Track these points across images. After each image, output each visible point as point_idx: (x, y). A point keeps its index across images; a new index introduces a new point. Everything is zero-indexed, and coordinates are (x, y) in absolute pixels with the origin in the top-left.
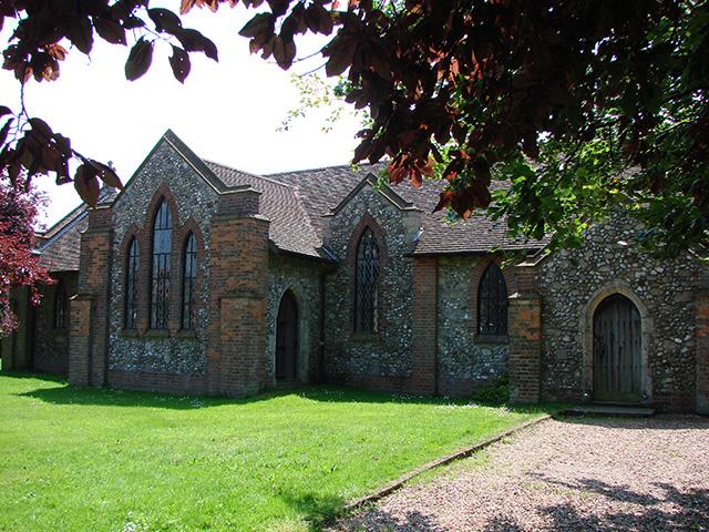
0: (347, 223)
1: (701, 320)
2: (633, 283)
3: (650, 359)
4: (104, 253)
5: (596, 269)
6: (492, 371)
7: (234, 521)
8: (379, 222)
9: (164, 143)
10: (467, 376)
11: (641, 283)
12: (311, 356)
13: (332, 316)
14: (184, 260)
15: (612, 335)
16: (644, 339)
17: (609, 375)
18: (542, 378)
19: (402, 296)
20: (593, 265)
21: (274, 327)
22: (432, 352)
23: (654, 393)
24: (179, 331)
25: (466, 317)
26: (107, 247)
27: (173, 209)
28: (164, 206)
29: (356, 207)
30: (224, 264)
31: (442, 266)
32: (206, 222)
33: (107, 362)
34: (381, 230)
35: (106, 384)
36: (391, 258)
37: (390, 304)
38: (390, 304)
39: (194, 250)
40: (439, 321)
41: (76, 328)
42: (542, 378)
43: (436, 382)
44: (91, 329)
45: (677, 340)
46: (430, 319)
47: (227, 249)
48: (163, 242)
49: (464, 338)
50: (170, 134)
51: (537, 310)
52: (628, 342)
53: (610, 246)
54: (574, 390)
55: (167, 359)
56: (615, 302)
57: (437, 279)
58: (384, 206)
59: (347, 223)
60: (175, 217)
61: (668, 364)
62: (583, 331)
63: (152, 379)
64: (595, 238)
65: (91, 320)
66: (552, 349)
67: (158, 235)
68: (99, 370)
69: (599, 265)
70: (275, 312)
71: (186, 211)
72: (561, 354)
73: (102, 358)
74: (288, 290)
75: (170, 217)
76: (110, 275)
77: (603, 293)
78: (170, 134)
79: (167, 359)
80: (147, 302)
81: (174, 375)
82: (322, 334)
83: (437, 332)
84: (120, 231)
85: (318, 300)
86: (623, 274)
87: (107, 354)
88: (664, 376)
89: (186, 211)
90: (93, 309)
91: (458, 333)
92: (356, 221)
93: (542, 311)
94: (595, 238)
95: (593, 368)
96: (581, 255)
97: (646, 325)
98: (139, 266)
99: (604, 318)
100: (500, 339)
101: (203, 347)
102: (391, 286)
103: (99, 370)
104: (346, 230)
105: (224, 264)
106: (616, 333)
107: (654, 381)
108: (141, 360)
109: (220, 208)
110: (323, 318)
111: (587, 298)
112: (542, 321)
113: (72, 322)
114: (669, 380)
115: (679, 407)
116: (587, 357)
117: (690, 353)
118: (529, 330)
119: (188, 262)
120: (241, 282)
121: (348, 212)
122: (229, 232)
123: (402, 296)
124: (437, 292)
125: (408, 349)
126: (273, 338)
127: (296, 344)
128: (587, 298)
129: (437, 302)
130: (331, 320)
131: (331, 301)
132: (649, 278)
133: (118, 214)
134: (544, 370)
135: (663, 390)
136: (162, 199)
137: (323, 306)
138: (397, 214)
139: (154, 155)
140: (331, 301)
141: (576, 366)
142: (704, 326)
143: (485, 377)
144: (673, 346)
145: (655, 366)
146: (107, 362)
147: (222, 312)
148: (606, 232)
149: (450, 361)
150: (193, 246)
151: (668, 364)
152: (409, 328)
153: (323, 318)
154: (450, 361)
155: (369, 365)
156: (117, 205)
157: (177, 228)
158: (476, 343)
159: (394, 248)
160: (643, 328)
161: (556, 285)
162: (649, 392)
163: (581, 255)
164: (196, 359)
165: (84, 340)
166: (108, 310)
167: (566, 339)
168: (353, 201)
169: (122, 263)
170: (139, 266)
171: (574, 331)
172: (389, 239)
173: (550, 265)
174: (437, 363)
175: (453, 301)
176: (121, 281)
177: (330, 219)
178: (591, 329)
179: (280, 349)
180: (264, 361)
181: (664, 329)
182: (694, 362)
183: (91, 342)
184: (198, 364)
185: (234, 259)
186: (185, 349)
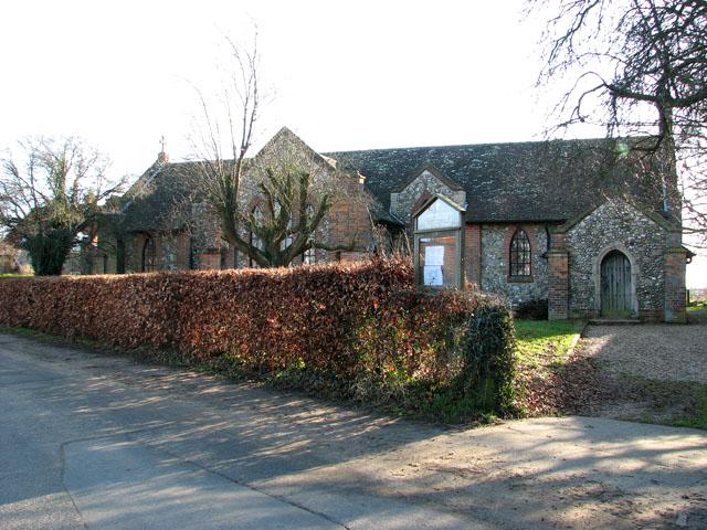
5: (603, 235)
11: (632, 244)
16: (633, 278)
18: (569, 302)
40: (482, 267)
42: (569, 302)
50: (285, 132)
61: (648, 293)
72: (581, 288)
77: (605, 250)
86: (622, 238)
92: (418, 196)
97: (635, 269)
141: (591, 294)
151: (648, 293)
160: (633, 271)
161: (579, 244)
173: (574, 231)
175: (492, 253)
181: (646, 271)
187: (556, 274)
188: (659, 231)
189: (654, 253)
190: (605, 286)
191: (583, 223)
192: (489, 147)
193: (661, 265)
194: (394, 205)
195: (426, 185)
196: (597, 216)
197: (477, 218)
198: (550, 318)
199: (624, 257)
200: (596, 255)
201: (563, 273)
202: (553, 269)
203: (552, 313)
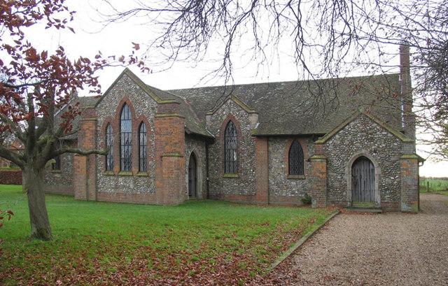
4: (92, 131)
7: (183, 282)
9: (125, 75)
11: (375, 152)
12: (203, 185)
13: (213, 165)
19: (249, 156)
22: (266, 183)
26: (94, 128)
27: (131, 107)
30: (163, 138)
32: (151, 117)
40: (269, 168)
46: (265, 167)
48: (127, 127)
49: (282, 176)
53: (360, 134)
55: (132, 186)
56: (361, 160)
60: (133, 114)
61: (388, 189)
68: (92, 191)
72: (337, 184)
74: (193, 152)
75: (130, 114)
77: (356, 154)
84: (101, 120)
86: (366, 147)
92: (224, 118)
97: (377, 171)
99: (357, 167)
100: (300, 177)
101: (152, 180)
106: (363, 175)
108: (116, 187)
109: (159, 111)
116: (349, 186)
126: (187, 176)
127: (196, 179)
134: (328, 190)
136: (125, 103)
137: (207, 159)
150: (144, 129)
151: (388, 189)
157: (134, 120)
160: (376, 172)
164: (149, 186)
167: (339, 177)
171: (343, 174)
173: (331, 142)
179: (190, 181)
181: (386, 173)
182: (400, 188)
186: (141, 181)
188: (396, 141)
189: (393, 159)
191: (337, 136)
192: (279, 84)
197: (264, 133)
201: (323, 173)
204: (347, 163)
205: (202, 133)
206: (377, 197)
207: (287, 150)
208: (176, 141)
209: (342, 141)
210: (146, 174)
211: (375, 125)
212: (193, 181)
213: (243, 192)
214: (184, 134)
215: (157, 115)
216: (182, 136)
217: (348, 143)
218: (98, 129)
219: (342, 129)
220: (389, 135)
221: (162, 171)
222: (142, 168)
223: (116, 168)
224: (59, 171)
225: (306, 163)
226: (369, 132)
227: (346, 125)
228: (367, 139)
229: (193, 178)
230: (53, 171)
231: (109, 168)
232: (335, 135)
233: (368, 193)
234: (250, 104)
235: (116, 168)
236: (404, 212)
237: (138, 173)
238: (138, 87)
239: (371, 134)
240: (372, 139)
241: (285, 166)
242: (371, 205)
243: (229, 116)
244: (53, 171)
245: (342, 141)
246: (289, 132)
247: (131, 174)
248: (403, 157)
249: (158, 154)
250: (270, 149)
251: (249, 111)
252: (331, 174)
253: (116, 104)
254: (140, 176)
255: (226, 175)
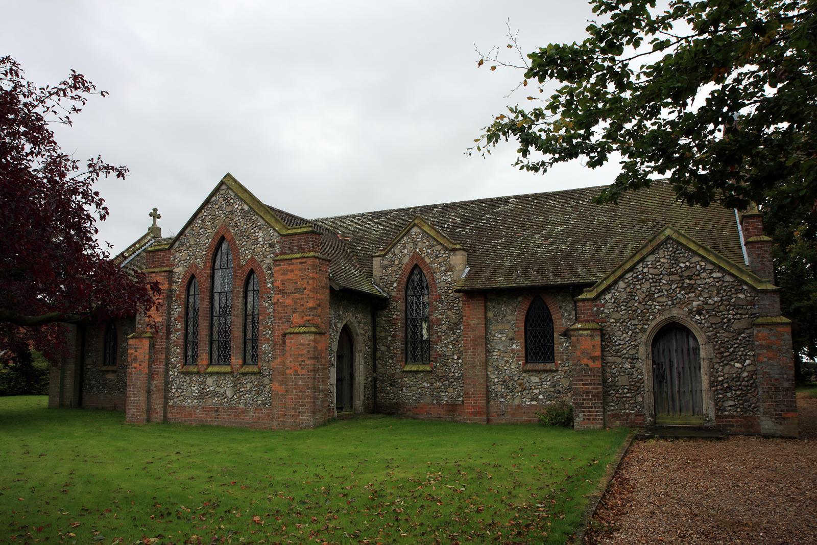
0: (397, 262)
1: (761, 345)
2: (690, 312)
3: (711, 384)
5: (653, 300)
6: (541, 397)
8: (428, 261)
9: (224, 187)
10: (517, 402)
11: (699, 312)
13: (383, 348)
14: (246, 297)
15: (671, 362)
16: (704, 365)
17: (670, 399)
18: (605, 403)
19: (451, 329)
20: (651, 296)
21: (334, 360)
23: (717, 416)
24: (241, 367)
25: (514, 347)
27: (233, 248)
28: (224, 246)
29: (404, 247)
30: (288, 300)
31: (430, 315)
32: (268, 261)
33: (166, 398)
34: (430, 269)
35: (165, 420)
36: (440, 295)
37: (440, 337)
38: (440, 337)
39: (255, 288)
40: (488, 352)
41: (134, 365)
42: (605, 403)
43: (488, 408)
44: (150, 366)
45: (737, 365)
46: (480, 351)
47: (290, 287)
48: (224, 281)
50: (228, 175)
51: (598, 339)
52: (687, 366)
53: (666, 278)
54: (637, 415)
55: (229, 393)
57: (486, 313)
58: (432, 246)
59: (397, 262)
60: (237, 257)
61: (729, 388)
62: (644, 358)
63: (214, 414)
64: (652, 271)
65: (150, 357)
66: (614, 376)
67: (218, 274)
68: (158, 406)
69: (656, 296)
70: (335, 347)
71: (247, 252)
72: (623, 380)
73: (161, 395)
76: (169, 313)
77: (655, 322)
78: (228, 175)
79: (229, 393)
80: (208, 338)
81: (237, 409)
82: (375, 366)
83: (487, 361)
84: (179, 270)
85: (370, 333)
86: (681, 303)
87: (166, 390)
88: (725, 399)
89: (247, 252)
90: (153, 346)
91: (507, 362)
92: (406, 260)
93: (602, 341)
94: (652, 271)
95: (654, 393)
96: (638, 287)
97: (705, 352)
98: (202, 305)
99: (662, 345)
100: (548, 366)
101: (266, 381)
102: (441, 320)
103: (158, 406)
104: (395, 268)
105: (288, 300)
107: (716, 404)
108: (202, 395)
109: (282, 247)
110: (375, 350)
111: (646, 327)
112: (603, 349)
113: (129, 359)
114: (731, 403)
115: (743, 429)
117: (750, 377)
118: (591, 358)
119: (250, 300)
120: (306, 318)
121: (397, 252)
122: (292, 270)
123: (451, 329)
124: (486, 324)
125: (459, 378)
126: (334, 370)
128: (646, 327)
129: (486, 334)
130: (383, 353)
131: (383, 334)
132: (706, 307)
133: (177, 254)
134: (606, 394)
135: (726, 413)
136: (223, 239)
137: (374, 339)
138: (445, 253)
139: (214, 198)
140: (383, 334)
141: (638, 391)
142: (765, 351)
143: (534, 403)
144: (733, 371)
145: (717, 390)
146: (166, 398)
147: (287, 348)
148: (662, 265)
149: (500, 388)
151: (729, 388)
152: (459, 358)
153: (375, 350)
154: (500, 388)
155: (421, 394)
156: (176, 246)
158: (525, 371)
159: (442, 284)
160: (703, 354)
161: (615, 316)
162: (712, 415)
163: (638, 287)
165: (143, 376)
166: (168, 347)
167: (627, 366)
168: (403, 242)
169: (183, 301)
170: (202, 305)
171: (635, 358)
172: (437, 275)
173: (608, 297)
174: (488, 391)
175: (501, 332)
176: (182, 318)
177: (380, 258)
178: (650, 356)
179: (339, 380)
180: (328, 394)
181: (723, 355)
182: (754, 386)
183: (150, 377)
184: (261, 399)
185: (298, 296)
186: (247, 384)
187: (584, 361)
188: (742, 291)
189: (736, 326)
190: (659, 377)
191: (621, 284)
192: (505, 200)
193: (749, 343)
194: (377, 272)
195: (415, 245)
196: (642, 273)
197: (479, 285)
198: (576, 426)
199: (687, 332)
200: (643, 331)
201: (593, 359)
202: (578, 353)
203: (579, 419)
204: (643, 338)
205: (365, 288)
206: (708, 405)
207: (522, 317)
208: (311, 304)
209: (631, 295)
210: (256, 370)
211: (696, 259)
212: (345, 380)
213: (439, 398)
214: (328, 291)
215: (279, 257)
216: (325, 295)
217: (642, 296)
218: (174, 287)
219: (631, 269)
220: (727, 278)
221: (284, 363)
222: (249, 357)
223: (203, 359)
224: (114, 368)
225: (558, 338)
226: (686, 274)
227: (638, 263)
228: (682, 288)
229: (346, 374)
230: (104, 368)
231: (190, 360)
232: (616, 282)
233: (688, 397)
234: (454, 236)
235: (203, 359)
236: (766, 437)
237: (241, 367)
238: (246, 207)
239: (690, 278)
240: (692, 288)
241: (517, 346)
242: (695, 421)
243: (415, 256)
244: (104, 368)
245: (631, 295)
246: (525, 282)
247: (228, 369)
248: (759, 321)
249: (279, 331)
250: (490, 314)
251: (451, 246)
252: (610, 359)
253: (206, 241)
254: (244, 374)
255: (407, 368)
